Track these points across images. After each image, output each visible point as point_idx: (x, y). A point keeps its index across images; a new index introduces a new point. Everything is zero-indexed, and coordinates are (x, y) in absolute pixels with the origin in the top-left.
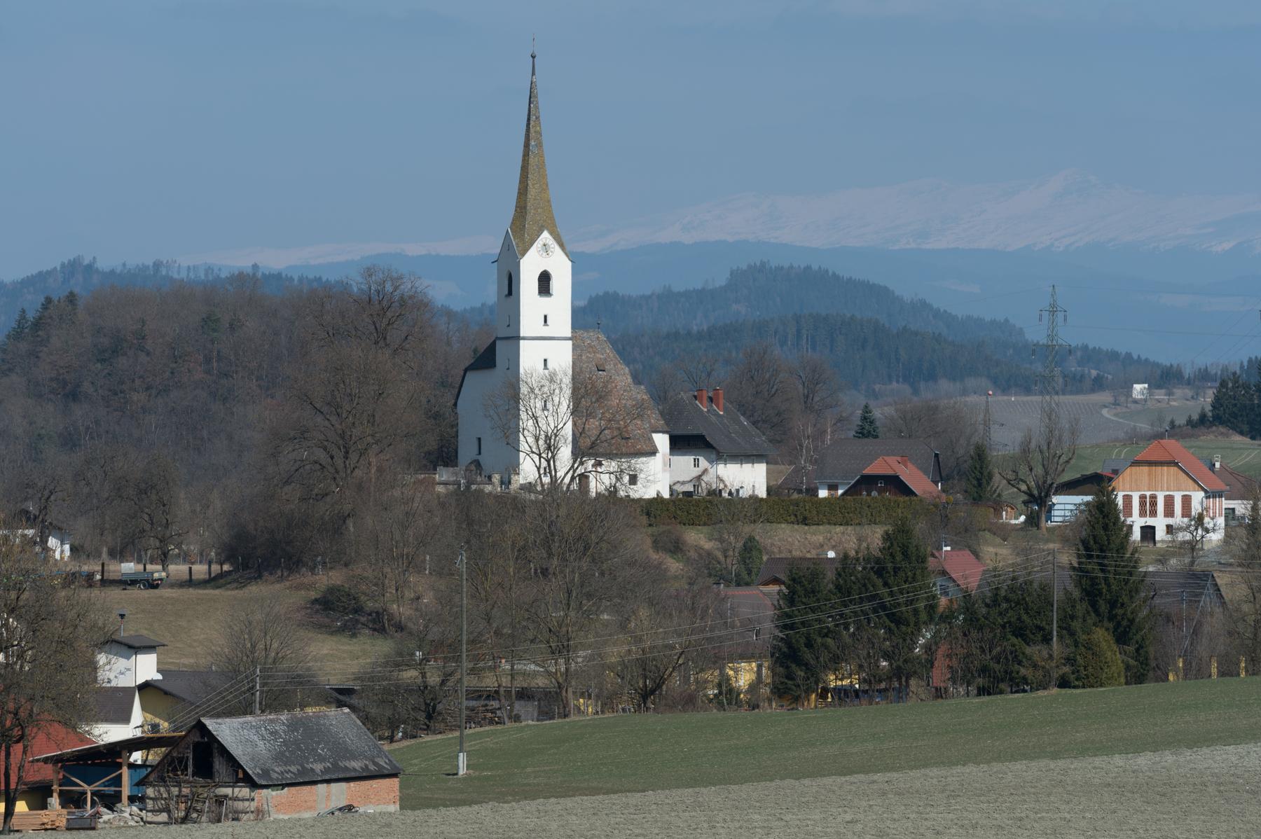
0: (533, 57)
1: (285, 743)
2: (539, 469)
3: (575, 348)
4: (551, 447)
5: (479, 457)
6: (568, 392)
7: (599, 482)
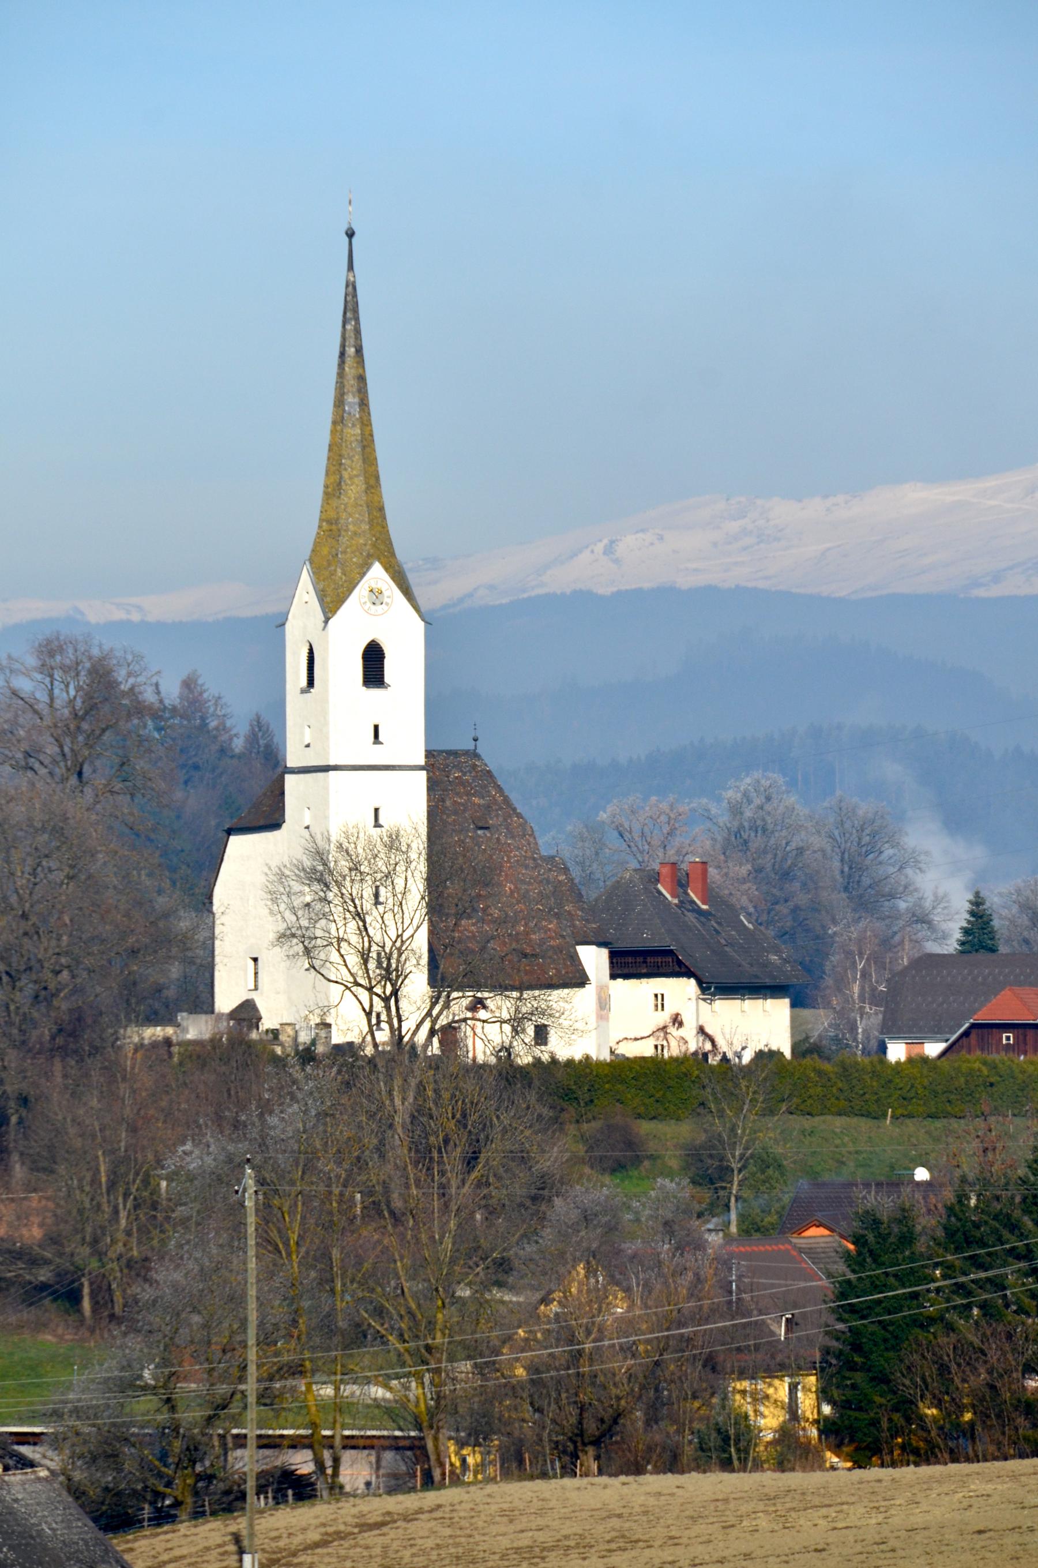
0: (350, 234)
2: (368, 1014)
3: (432, 786)
4: (392, 975)
5: (254, 996)
6: (421, 867)
7: (486, 1038)
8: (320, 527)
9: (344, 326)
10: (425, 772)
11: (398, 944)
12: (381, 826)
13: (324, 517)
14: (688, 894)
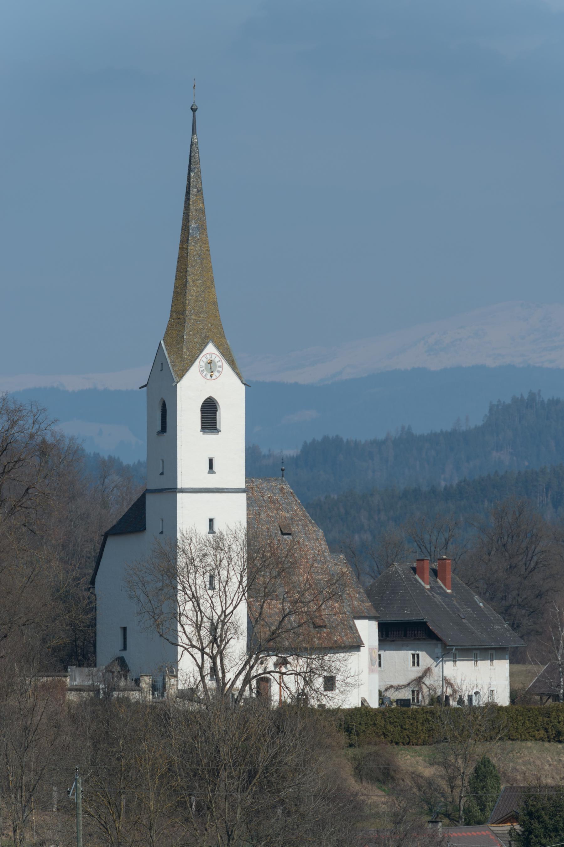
0: (194, 110)
8: (171, 316)
9: (189, 174)
10: (244, 495)
11: (222, 618)
12: (214, 533)
13: (174, 309)
14: (437, 582)
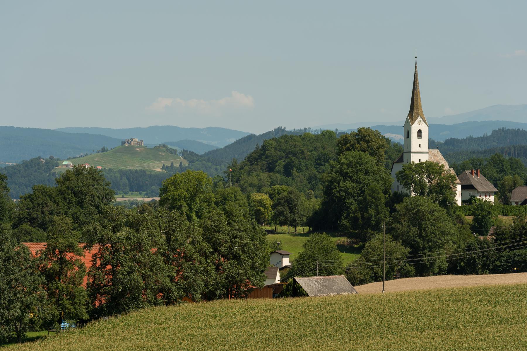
1: (322, 286)
